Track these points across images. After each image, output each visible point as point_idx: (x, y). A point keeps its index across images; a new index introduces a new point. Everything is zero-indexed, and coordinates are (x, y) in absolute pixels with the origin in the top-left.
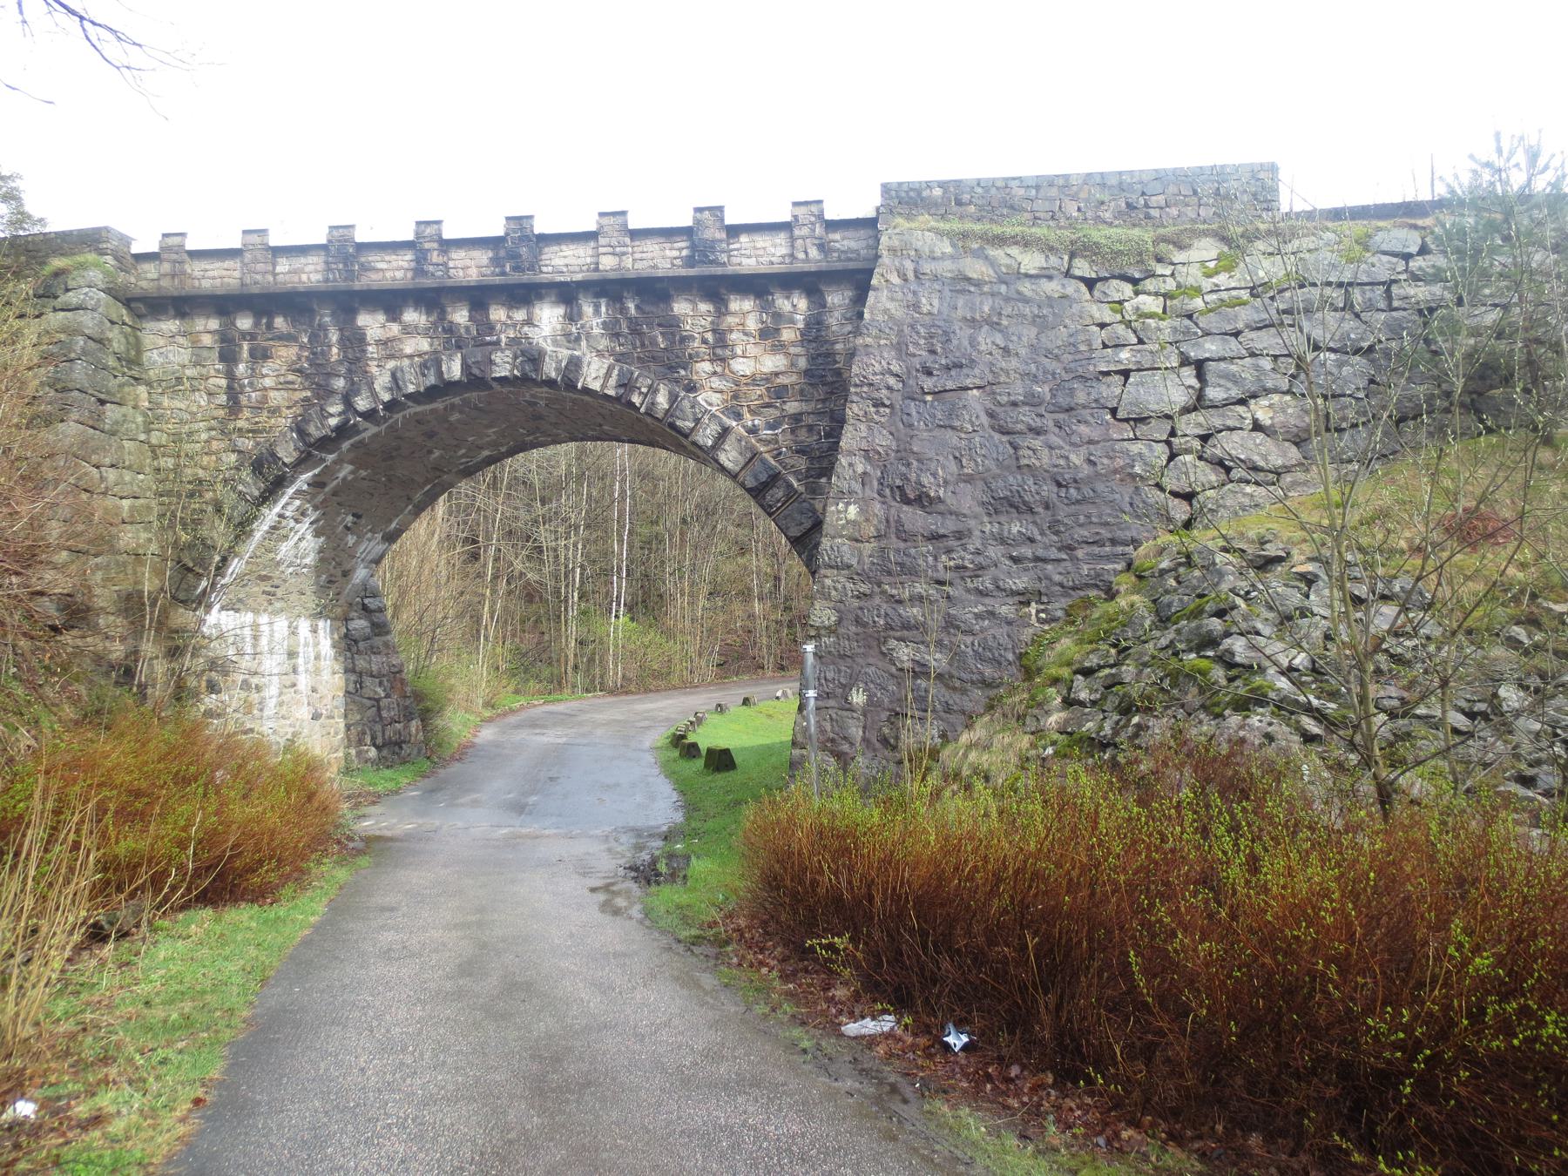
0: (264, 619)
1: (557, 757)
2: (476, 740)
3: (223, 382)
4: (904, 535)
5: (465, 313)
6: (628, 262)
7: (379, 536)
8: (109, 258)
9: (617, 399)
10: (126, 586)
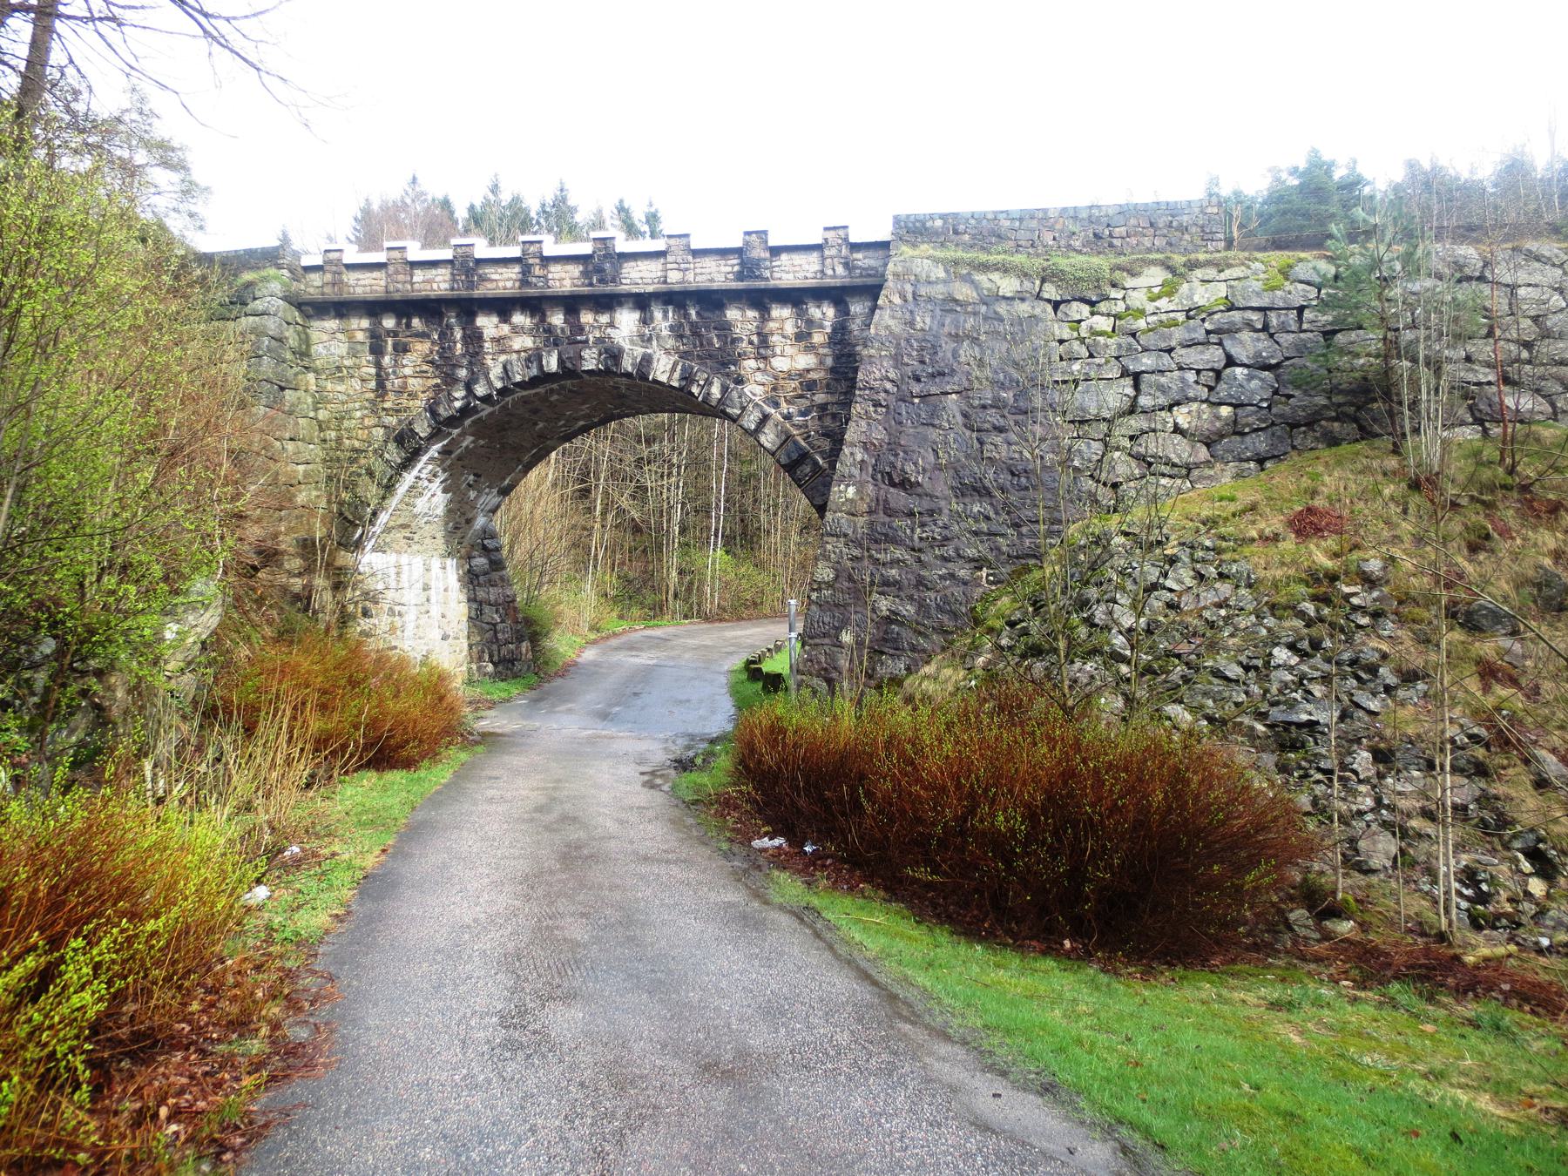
0: (404, 559)
1: (645, 675)
2: (579, 660)
3: (373, 371)
4: (890, 512)
5: (561, 316)
6: (690, 276)
7: (495, 491)
8: (285, 272)
9: (681, 389)
10: (302, 534)
